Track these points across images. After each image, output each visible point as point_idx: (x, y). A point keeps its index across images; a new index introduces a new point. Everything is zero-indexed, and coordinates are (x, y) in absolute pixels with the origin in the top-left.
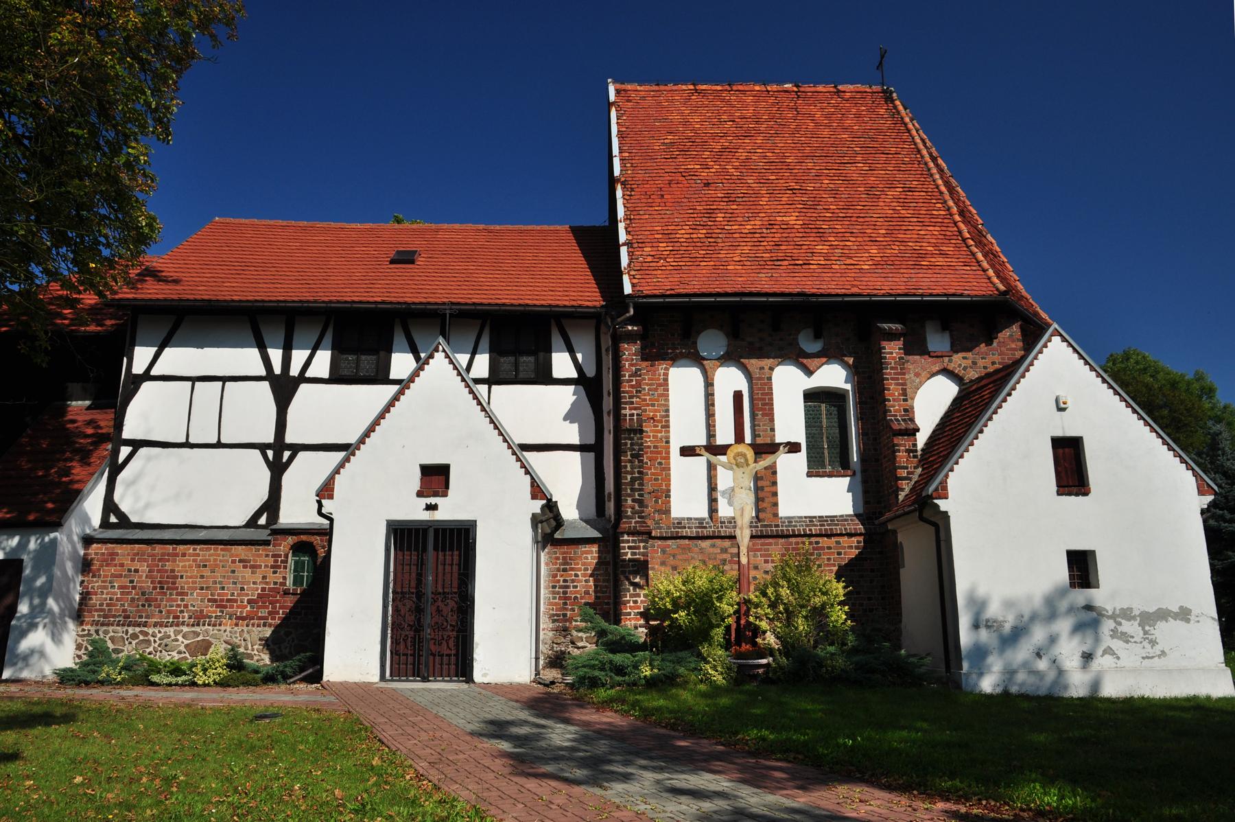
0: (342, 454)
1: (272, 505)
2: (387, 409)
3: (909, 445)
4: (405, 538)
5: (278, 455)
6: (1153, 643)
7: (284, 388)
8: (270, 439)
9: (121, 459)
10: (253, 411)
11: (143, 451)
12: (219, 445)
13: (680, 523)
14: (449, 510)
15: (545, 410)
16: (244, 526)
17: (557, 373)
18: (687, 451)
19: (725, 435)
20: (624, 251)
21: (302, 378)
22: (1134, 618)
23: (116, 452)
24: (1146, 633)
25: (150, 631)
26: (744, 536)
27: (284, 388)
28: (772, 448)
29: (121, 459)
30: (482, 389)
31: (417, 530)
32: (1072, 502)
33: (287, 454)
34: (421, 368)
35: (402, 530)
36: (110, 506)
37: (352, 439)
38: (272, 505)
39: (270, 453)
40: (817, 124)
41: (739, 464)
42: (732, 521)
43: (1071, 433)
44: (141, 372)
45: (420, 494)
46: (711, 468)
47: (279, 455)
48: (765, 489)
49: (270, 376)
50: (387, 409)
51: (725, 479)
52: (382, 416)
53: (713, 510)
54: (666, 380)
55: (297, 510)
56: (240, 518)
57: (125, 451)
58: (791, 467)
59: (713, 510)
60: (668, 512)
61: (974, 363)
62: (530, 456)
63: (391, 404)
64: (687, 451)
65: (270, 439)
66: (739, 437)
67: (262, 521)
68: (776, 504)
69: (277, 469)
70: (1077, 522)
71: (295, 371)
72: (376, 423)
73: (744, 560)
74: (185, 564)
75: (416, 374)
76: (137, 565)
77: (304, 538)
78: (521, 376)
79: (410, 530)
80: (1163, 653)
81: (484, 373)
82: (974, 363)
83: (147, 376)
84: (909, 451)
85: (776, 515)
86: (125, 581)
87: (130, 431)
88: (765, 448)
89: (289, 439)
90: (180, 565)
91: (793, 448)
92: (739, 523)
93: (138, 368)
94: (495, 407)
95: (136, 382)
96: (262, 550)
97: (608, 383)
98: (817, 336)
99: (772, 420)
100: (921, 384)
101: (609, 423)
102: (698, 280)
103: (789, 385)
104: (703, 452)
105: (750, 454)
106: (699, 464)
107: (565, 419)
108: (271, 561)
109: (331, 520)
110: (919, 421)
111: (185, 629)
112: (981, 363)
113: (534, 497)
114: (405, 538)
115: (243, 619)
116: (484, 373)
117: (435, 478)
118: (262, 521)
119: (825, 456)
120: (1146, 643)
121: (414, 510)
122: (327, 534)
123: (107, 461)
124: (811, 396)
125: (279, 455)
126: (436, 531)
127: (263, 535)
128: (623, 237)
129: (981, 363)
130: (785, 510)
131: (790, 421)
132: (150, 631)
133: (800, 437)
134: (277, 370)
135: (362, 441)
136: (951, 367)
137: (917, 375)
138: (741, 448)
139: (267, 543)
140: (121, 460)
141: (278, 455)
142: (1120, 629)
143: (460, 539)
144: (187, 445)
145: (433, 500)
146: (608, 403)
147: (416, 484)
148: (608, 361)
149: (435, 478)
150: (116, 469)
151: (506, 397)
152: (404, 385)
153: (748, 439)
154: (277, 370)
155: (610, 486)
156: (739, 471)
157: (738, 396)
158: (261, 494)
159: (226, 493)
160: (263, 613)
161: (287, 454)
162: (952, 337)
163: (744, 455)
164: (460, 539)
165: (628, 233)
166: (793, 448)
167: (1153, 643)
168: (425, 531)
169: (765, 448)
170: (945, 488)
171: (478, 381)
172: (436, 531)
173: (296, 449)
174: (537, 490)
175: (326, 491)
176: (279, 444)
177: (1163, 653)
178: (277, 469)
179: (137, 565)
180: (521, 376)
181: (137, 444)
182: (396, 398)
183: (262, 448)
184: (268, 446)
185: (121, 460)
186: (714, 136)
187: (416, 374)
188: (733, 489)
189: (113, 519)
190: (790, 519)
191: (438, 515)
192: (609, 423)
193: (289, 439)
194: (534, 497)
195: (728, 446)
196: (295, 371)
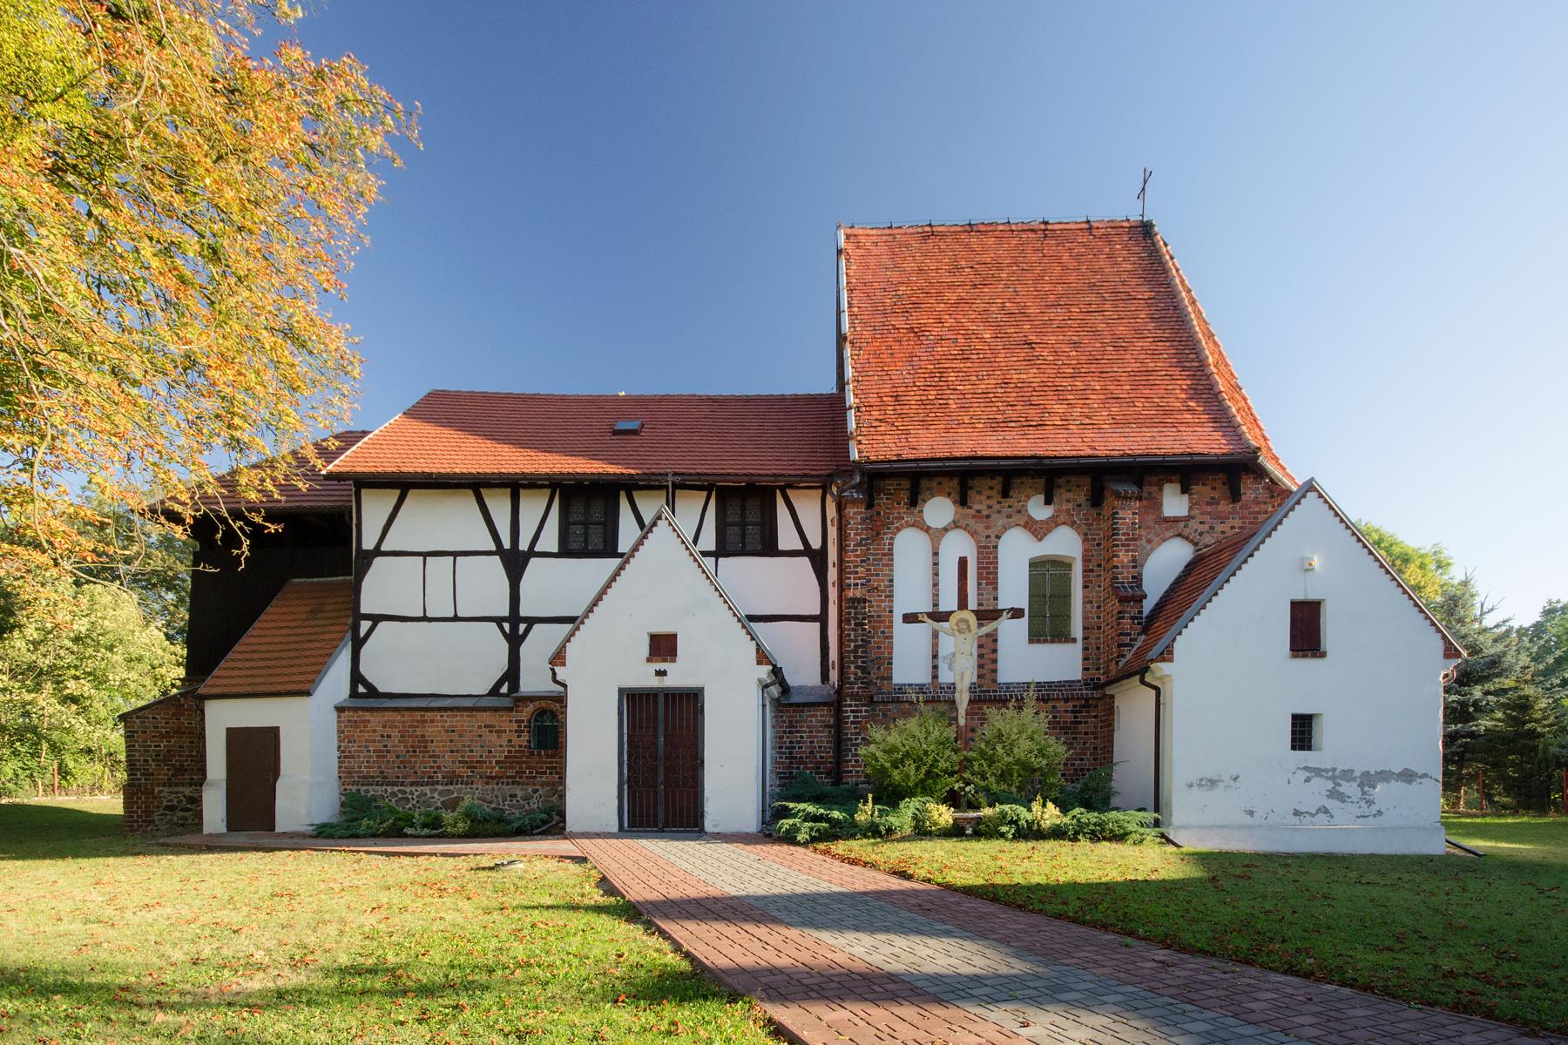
0: (569, 627)
1: (512, 674)
2: (613, 579)
3: (1134, 612)
4: (636, 703)
5: (514, 628)
6: (1370, 803)
7: (515, 562)
8: (505, 612)
9: (362, 633)
10: (486, 585)
11: (382, 625)
12: (456, 618)
13: (901, 689)
14: (678, 676)
15: (781, 582)
16: (564, 646)
17: (783, 545)
18: (910, 618)
19: (949, 601)
20: (851, 415)
21: (532, 553)
22: (1354, 779)
23: (356, 628)
24: (1364, 793)
25: (408, 789)
26: (963, 699)
27: (515, 562)
28: (995, 614)
29: (362, 633)
30: (709, 562)
31: (648, 695)
32: (1308, 664)
33: (522, 627)
34: (645, 537)
35: (634, 696)
36: (357, 677)
37: (577, 612)
38: (512, 674)
39: (506, 626)
40: (1065, 268)
41: (963, 628)
42: (952, 687)
43: (1312, 596)
44: (371, 547)
45: (649, 660)
46: (935, 635)
47: (515, 627)
48: (988, 652)
49: (500, 551)
50: (613, 579)
51: (947, 645)
52: (608, 585)
53: (935, 677)
54: (891, 549)
55: (534, 680)
56: (484, 688)
57: (365, 626)
58: (1013, 633)
59: (935, 677)
60: (890, 678)
61: (1212, 528)
62: (754, 626)
63: (617, 574)
64: (910, 618)
65: (505, 612)
66: (963, 604)
67: (504, 689)
68: (995, 671)
69: (515, 642)
70: (1306, 685)
71: (524, 545)
72: (603, 592)
73: (962, 721)
74: (435, 730)
75: (640, 542)
76: (388, 731)
77: (543, 704)
78: (748, 548)
79: (641, 695)
80: (1380, 813)
81: (712, 547)
82: (1212, 528)
83: (378, 552)
84: (1133, 618)
85: (994, 681)
86: (380, 746)
87: (370, 602)
88: (988, 615)
89: (523, 612)
90: (429, 731)
91: (1017, 613)
92: (958, 687)
93: (368, 543)
94: (721, 580)
95: (368, 558)
96: (505, 716)
97: (832, 555)
98: (1048, 502)
99: (996, 589)
100: (1152, 550)
101: (833, 593)
102: (927, 444)
103: (1017, 552)
104: (926, 618)
105: (973, 620)
106: (922, 631)
107: (1323, 655)
108: (515, 726)
109: (565, 686)
110: (1147, 586)
111: (440, 788)
112: (1219, 528)
113: (759, 663)
114: (636, 703)
115: (493, 778)
116: (712, 547)
117: (663, 647)
118: (504, 689)
119: (1047, 624)
120: (1363, 803)
121: (644, 676)
122: (561, 700)
123: (349, 635)
124: (1036, 565)
125: (515, 627)
126: (666, 696)
127: (506, 702)
128: (851, 400)
129: (1219, 528)
130: (1003, 677)
131: (1014, 589)
132: (408, 789)
133: (1023, 602)
134: (507, 545)
135: (590, 610)
136: (1186, 532)
137: (1149, 541)
138: (965, 614)
139: (510, 709)
140: (362, 634)
141: (514, 628)
142: (1341, 789)
143: (689, 702)
144: (425, 619)
145: (662, 666)
146: (832, 574)
147: (645, 650)
148: (833, 532)
149: (663, 647)
150: (358, 644)
151: (738, 569)
152: (626, 558)
153: (972, 603)
154: (507, 545)
155: (833, 655)
156: (960, 637)
157: (963, 563)
158: (501, 664)
159: (464, 664)
160: (511, 773)
161: (522, 627)
162: (1190, 500)
163: (966, 621)
164: (689, 702)
165: (856, 395)
166: (1017, 613)
167: (1370, 803)
168: (656, 696)
169: (988, 615)
170: (1171, 652)
171: (705, 554)
172: (666, 696)
173: (531, 621)
174: (762, 657)
175: (558, 658)
176: (514, 617)
177: (1380, 813)
178: (515, 642)
179: (388, 731)
180: (748, 548)
181: (376, 619)
182: (622, 568)
183: (499, 621)
184: (504, 619)
185: (362, 634)
186: (951, 285)
187: (640, 542)
188: (954, 655)
189: (361, 689)
190: (1008, 685)
191: (670, 682)
192: (833, 593)
193: (523, 612)
194: (759, 663)
195: (951, 613)
196: (524, 545)
